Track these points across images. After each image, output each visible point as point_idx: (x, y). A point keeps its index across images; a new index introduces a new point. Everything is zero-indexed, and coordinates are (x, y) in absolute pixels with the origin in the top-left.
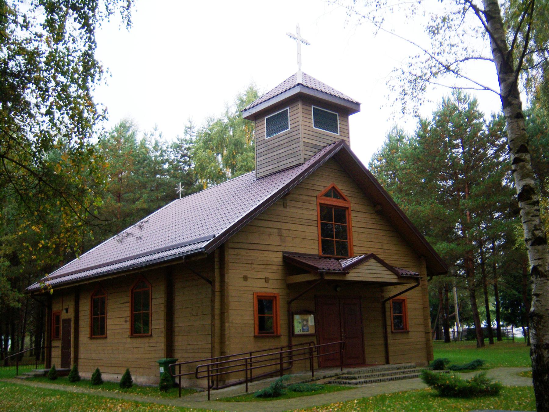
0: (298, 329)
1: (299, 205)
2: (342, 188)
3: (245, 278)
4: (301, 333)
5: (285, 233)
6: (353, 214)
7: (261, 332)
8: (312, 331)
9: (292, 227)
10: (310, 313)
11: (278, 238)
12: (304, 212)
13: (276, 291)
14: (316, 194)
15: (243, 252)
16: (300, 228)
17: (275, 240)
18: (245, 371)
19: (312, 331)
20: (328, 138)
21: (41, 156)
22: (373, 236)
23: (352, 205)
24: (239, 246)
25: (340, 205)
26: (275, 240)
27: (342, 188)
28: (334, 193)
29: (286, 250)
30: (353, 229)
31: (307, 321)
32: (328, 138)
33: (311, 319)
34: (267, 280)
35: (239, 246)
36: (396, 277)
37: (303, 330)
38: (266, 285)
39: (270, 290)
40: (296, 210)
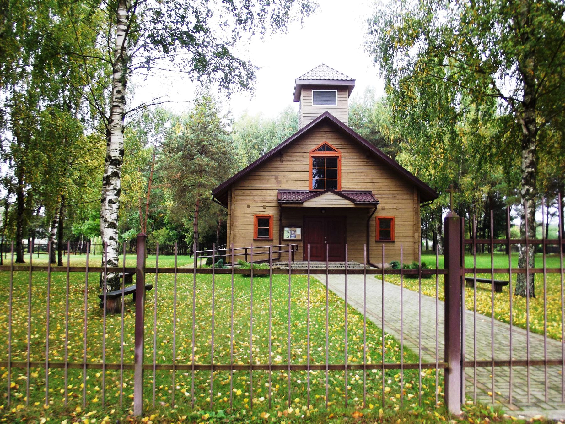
0: (287, 236)
1: (294, 159)
2: (332, 143)
3: (249, 207)
4: (290, 238)
5: (280, 178)
6: (343, 160)
7: (88, 251)
8: (300, 238)
9: (286, 174)
10: (298, 227)
11: (275, 181)
12: (298, 163)
13: (271, 214)
14: (309, 150)
15: (248, 192)
16: (294, 174)
17: (273, 183)
18: (268, 255)
19: (300, 238)
20: (321, 110)
21: (485, 149)
22: (362, 174)
23: (342, 154)
24: (245, 188)
25: (334, 155)
26: (273, 183)
27: (332, 143)
28: (326, 147)
29: (281, 188)
30: (342, 171)
31: (295, 231)
32: (321, 110)
33: (298, 231)
34: (265, 207)
35: (245, 188)
36: (353, 204)
37: (291, 237)
38: (264, 210)
39: (268, 213)
40: (291, 163)
